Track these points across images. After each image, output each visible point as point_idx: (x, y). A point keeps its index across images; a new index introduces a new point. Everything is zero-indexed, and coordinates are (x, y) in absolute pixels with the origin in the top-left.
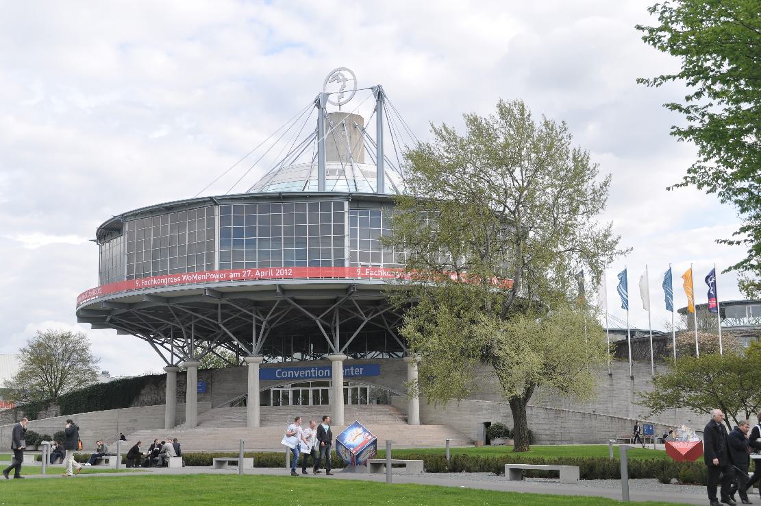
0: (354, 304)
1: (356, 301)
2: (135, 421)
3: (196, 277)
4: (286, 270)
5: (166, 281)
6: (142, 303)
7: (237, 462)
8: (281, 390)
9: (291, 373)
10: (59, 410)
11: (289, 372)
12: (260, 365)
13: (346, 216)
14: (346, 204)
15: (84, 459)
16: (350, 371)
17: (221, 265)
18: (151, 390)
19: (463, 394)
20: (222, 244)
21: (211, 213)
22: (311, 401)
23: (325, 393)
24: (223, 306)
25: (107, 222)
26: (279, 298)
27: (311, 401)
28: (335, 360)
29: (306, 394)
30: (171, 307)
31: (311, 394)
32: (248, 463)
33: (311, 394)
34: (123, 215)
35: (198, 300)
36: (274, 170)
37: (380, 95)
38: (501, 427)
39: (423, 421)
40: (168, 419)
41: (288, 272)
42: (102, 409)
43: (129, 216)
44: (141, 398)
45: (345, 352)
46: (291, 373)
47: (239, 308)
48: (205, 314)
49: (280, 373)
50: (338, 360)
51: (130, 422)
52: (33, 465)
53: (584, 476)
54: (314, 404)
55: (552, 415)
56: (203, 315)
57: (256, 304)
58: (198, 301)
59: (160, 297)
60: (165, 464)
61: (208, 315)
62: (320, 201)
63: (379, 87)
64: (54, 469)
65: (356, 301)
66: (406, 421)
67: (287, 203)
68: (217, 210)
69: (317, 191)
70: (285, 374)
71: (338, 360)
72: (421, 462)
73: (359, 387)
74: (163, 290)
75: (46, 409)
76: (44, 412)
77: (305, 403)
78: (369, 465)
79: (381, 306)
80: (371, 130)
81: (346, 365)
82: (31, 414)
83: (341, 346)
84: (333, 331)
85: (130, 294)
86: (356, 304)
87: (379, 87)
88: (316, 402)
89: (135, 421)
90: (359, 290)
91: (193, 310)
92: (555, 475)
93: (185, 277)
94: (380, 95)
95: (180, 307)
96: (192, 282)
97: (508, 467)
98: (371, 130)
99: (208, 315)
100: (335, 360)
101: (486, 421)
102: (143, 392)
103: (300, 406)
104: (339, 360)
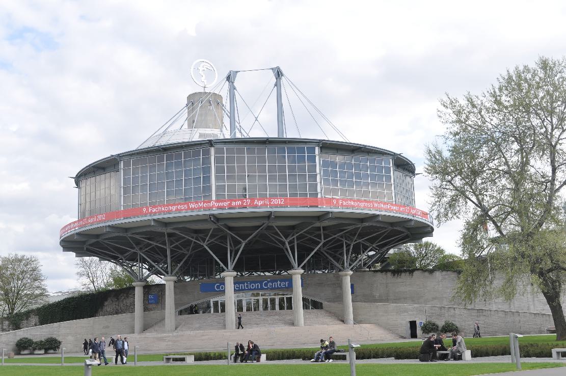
0: (275, 230)
1: (276, 226)
2: (107, 327)
3: (201, 205)
4: (279, 200)
5: (174, 208)
6: (150, 226)
7: (184, 358)
8: (285, 297)
9: (275, 284)
10: (37, 319)
11: (256, 284)
12: (235, 277)
13: (317, 158)
14: (317, 150)
15: (309, 355)
16: (277, 284)
17: (217, 195)
18: (112, 301)
19: (385, 299)
20: (217, 178)
21: (207, 153)
22: (277, 307)
23: (289, 300)
24: (170, 235)
25: (96, 162)
26: (212, 226)
27: (277, 307)
28: (295, 274)
29: (273, 301)
30: (130, 237)
31: (261, 302)
32: (190, 360)
33: (261, 302)
34: (119, 155)
35: (148, 229)
36: (157, 134)
37: (279, 74)
38: (434, 324)
39: (357, 321)
40: (138, 325)
41: (281, 201)
42: (79, 318)
43: (124, 156)
44: (105, 308)
45: (303, 268)
46: (275, 284)
47: (184, 236)
48: (158, 241)
49: (218, 287)
50: (297, 274)
51: (103, 328)
52: (265, 363)
53: (196, 360)
54: (214, 312)
55: (474, 313)
56: (157, 242)
57: (196, 231)
58: (144, 230)
59: (161, 222)
60: (460, 358)
61: (160, 242)
62: (296, 146)
63: (278, 68)
64: (169, 367)
65: (276, 226)
66: (293, 324)
67: (271, 146)
68: (212, 150)
69: (277, 137)
70: (253, 286)
71: (297, 274)
72: (193, 356)
73: (285, 297)
74: (171, 216)
75: (27, 319)
76: (25, 322)
77: (273, 308)
78: (164, 359)
79: (295, 231)
80: (226, 102)
81: (236, 281)
82: (15, 324)
83: (299, 265)
84: (285, 251)
85: (127, 221)
86: (129, 239)
87: (278, 68)
88: (281, 308)
89: (107, 327)
90: (276, 217)
91: (149, 239)
92: (183, 360)
93: (192, 206)
94: (279, 74)
95: (137, 237)
96: (199, 208)
97: (554, 351)
98: (226, 102)
99: (160, 242)
100: (295, 274)
101: (411, 320)
102: (106, 303)
103: (285, 311)
104: (298, 274)
